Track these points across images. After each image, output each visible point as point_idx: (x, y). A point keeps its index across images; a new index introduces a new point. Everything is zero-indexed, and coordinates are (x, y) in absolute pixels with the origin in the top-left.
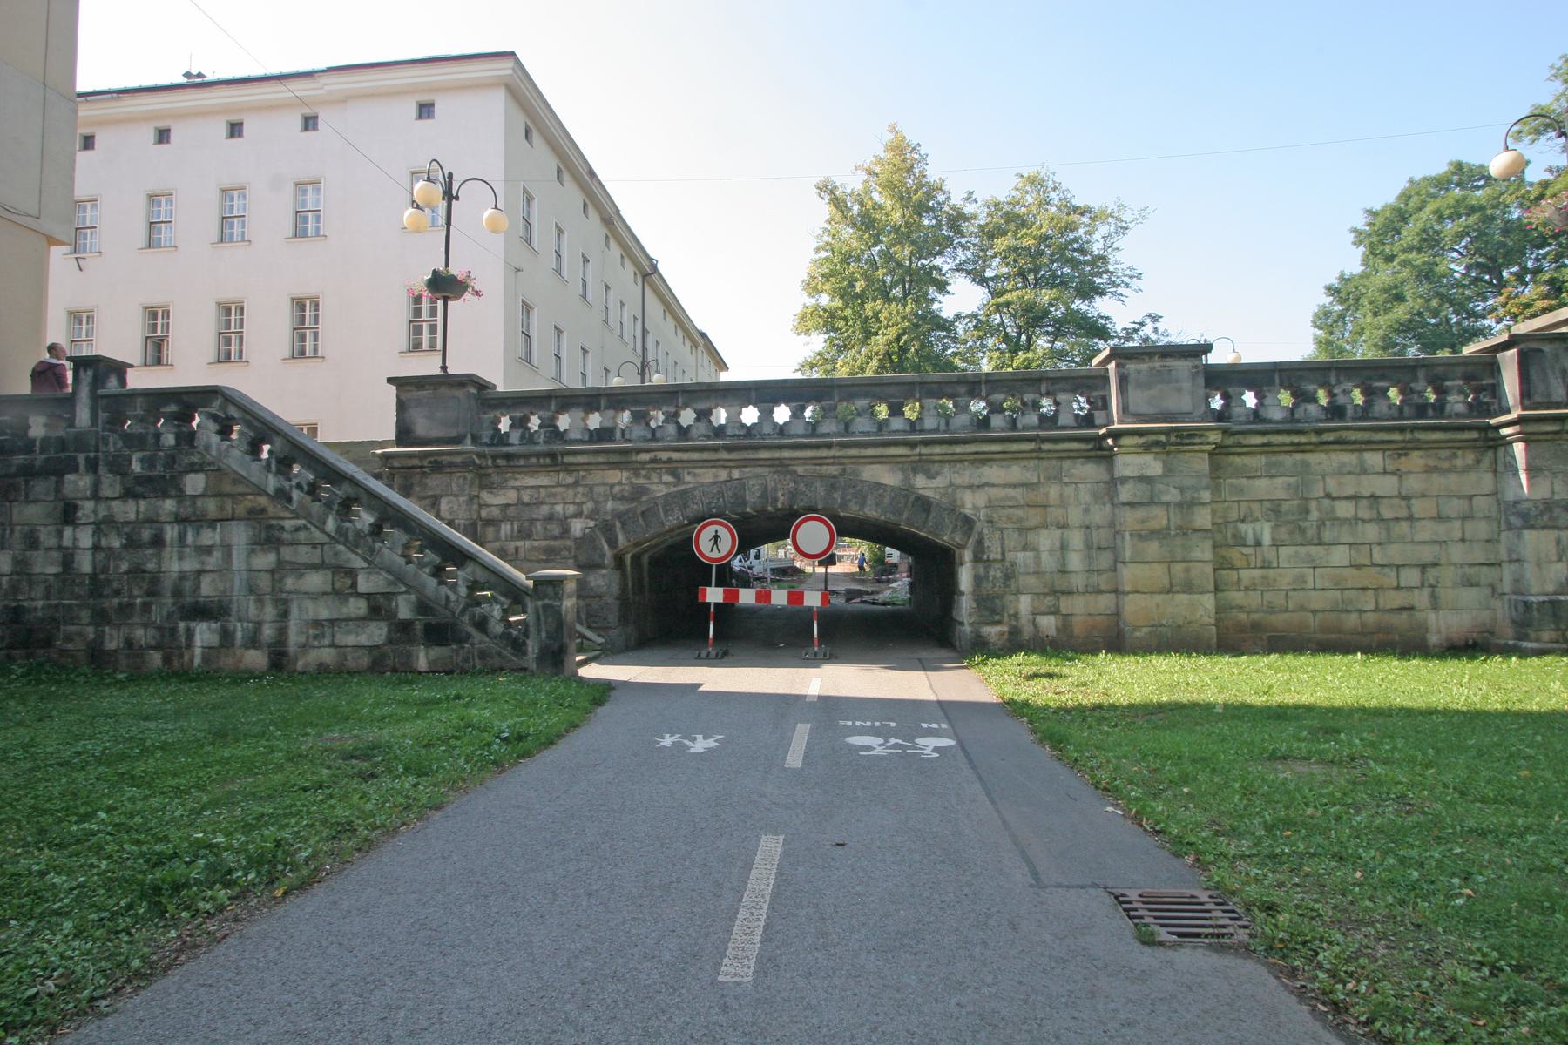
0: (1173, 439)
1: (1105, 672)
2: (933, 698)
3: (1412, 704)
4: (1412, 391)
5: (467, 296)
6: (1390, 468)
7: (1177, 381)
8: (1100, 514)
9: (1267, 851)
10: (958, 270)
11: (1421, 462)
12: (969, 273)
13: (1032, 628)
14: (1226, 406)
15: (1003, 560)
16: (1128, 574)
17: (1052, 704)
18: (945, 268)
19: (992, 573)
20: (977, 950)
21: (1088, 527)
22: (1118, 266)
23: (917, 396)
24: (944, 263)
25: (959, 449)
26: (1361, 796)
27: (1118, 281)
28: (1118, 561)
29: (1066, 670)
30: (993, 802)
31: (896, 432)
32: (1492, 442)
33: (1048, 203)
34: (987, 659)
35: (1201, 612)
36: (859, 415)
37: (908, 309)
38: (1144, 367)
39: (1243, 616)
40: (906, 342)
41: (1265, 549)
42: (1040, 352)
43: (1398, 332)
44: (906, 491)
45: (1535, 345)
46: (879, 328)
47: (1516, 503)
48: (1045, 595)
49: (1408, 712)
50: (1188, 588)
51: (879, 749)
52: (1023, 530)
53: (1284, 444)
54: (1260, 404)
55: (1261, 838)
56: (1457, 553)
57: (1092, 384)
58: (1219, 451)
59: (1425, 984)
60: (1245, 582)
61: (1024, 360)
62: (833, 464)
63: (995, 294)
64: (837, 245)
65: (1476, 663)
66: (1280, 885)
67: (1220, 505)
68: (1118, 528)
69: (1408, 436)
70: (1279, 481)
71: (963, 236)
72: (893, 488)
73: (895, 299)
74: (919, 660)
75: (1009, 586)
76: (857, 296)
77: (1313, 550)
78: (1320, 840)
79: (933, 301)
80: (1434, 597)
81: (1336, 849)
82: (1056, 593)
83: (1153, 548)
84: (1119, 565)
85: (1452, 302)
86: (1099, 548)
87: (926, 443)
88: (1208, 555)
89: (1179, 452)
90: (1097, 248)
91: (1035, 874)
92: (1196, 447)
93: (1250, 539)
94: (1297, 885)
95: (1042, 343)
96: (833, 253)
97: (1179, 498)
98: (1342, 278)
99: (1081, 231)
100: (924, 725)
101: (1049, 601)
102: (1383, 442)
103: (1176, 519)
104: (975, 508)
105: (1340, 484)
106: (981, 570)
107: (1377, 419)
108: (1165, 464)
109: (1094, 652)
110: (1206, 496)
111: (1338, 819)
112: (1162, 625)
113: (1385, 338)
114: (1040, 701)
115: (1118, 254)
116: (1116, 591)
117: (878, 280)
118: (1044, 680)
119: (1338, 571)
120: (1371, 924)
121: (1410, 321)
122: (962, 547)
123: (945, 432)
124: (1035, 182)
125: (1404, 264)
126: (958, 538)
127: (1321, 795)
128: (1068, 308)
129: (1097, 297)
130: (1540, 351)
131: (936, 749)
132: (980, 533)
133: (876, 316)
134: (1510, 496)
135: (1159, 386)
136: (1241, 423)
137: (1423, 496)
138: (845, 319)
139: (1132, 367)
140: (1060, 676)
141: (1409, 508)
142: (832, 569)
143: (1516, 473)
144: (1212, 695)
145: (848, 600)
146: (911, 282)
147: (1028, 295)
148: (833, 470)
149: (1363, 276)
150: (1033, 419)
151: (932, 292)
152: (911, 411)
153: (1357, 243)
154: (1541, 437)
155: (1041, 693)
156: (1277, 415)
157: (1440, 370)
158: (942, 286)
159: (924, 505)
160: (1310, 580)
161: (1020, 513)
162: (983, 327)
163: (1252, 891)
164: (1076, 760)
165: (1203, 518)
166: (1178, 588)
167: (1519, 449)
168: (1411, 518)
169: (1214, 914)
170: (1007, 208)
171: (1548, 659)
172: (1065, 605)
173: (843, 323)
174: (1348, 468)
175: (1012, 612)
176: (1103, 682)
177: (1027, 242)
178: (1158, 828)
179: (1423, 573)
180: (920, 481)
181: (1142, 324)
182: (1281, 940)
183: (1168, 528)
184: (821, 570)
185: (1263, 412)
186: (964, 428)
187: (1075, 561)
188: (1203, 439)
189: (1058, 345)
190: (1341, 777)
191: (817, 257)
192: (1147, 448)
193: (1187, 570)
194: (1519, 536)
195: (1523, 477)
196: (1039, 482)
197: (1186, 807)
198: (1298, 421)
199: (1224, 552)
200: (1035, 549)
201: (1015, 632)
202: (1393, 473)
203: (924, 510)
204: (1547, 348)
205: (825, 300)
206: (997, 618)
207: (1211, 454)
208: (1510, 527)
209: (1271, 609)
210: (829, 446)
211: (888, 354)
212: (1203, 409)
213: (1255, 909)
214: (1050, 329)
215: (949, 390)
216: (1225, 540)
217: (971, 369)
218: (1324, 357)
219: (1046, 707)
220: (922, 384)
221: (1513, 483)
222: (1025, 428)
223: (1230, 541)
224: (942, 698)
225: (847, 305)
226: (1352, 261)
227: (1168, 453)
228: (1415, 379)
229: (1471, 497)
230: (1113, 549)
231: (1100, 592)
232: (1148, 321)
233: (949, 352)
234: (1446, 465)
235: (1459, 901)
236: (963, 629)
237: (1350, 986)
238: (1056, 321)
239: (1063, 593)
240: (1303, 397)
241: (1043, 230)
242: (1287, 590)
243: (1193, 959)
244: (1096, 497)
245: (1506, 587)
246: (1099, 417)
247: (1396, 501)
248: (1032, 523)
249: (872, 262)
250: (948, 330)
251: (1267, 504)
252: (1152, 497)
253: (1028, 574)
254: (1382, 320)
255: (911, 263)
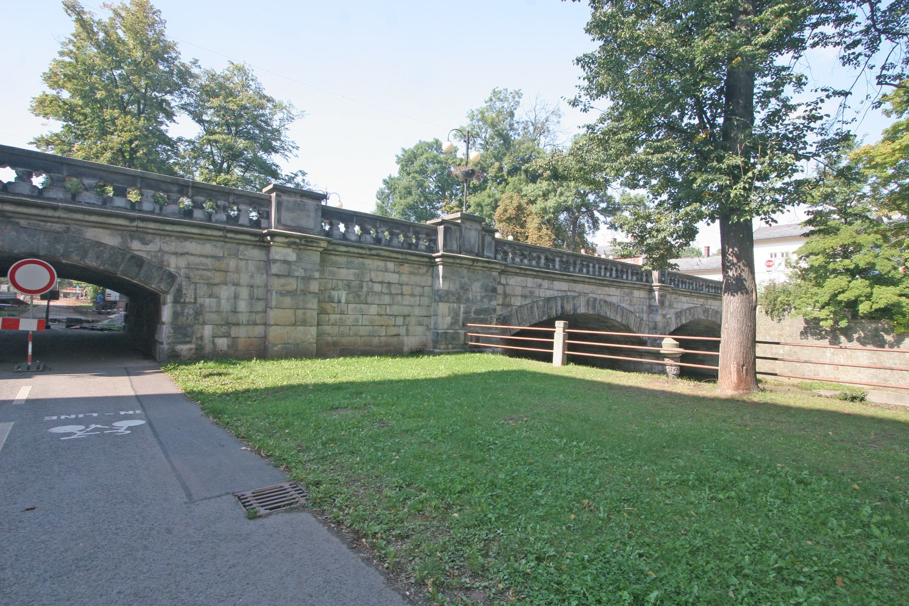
0: (303, 242)
1: (254, 371)
2: (132, 393)
3: (394, 378)
4: (408, 237)
5: (515, 111)
6: (396, 270)
7: (308, 211)
8: (259, 280)
9: (321, 456)
10: (182, 108)
11: (408, 269)
12: (190, 112)
13: (211, 346)
14: (331, 229)
15: (195, 303)
16: (273, 315)
17: (218, 391)
18: (173, 104)
19: (186, 311)
20: (140, 553)
21: (252, 286)
22: (287, 139)
23: (139, 185)
24: (174, 100)
25: (168, 228)
26: (366, 422)
27: (286, 147)
28: (268, 307)
29: (231, 371)
30: (167, 456)
31: (118, 208)
32: (432, 265)
33: (248, 87)
34: (178, 366)
35: (309, 336)
36: (86, 190)
37: (141, 123)
38: (291, 199)
39: (329, 339)
40: (137, 146)
41: (342, 304)
42: (235, 177)
43: (409, 209)
44: (123, 251)
45: (449, 226)
46: (115, 130)
47: (438, 291)
48: (222, 325)
49: (391, 382)
50: (304, 323)
51: (79, 433)
52: (210, 285)
53: (354, 253)
54: (346, 231)
55: (319, 450)
56: (417, 311)
57: (260, 203)
58: (325, 252)
59: (375, 501)
60: (332, 321)
61: (225, 179)
62: (57, 223)
63: (210, 132)
64: (81, 57)
65: (419, 359)
66: (325, 471)
67: (323, 280)
68: (269, 288)
69: (404, 257)
70: (352, 271)
71: (188, 87)
72: (112, 248)
73: (130, 112)
74: (125, 368)
75: (198, 320)
76: (96, 101)
77: (363, 306)
78: (345, 445)
79: (162, 123)
80: (407, 330)
81: (351, 448)
82: (228, 324)
83: (288, 301)
84: (268, 309)
85: (428, 201)
86: (258, 299)
87: (143, 220)
88: (315, 306)
89: (306, 249)
90: (275, 124)
91: (189, 496)
92: (314, 248)
93: (336, 300)
94: (332, 469)
95: (237, 172)
96: (77, 61)
97: (303, 275)
98: (390, 178)
99: (267, 111)
100: (122, 413)
101: (224, 329)
102: (395, 258)
103: (301, 286)
104: (178, 268)
105: (377, 275)
106: (179, 308)
107: (393, 247)
108: (298, 255)
109: (249, 359)
110: (317, 275)
111: (354, 434)
112: (289, 344)
113: (403, 210)
114: (211, 390)
115: (287, 132)
116: (265, 324)
117: (117, 95)
118: (216, 378)
119: (372, 317)
120: (359, 481)
121: (414, 205)
122: (167, 293)
123: (159, 214)
124: (240, 70)
125: (414, 178)
126: (163, 286)
127: (349, 424)
128: (255, 155)
129: (273, 153)
130: (450, 228)
131: (129, 428)
132: (180, 286)
133: (113, 120)
134: (436, 288)
135: (298, 212)
136: (337, 239)
137: (407, 284)
138: (85, 116)
139: (285, 198)
140: (226, 374)
141: (402, 289)
142: (52, 303)
143: (439, 279)
144: (310, 380)
145: (68, 327)
146: (145, 105)
147: (230, 140)
148: (57, 227)
149: (399, 179)
150: (223, 217)
151: (161, 117)
152: (133, 196)
153: (398, 163)
154: (212, 238)
155: (212, 385)
156: (353, 238)
157: (418, 229)
158: (170, 115)
159: (138, 262)
160: (361, 321)
161: (209, 274)
162: (198, 151)
163: (311, 477)
164: (228, 423)
165: (314, 286)
166: (299, 323)
167: (441, 267)
168: (402, 294)
169: (291, 493)
170: (221, 80)
171: (442, 356)
172: (234, 332)
173: (81, 117)
174: (380, 269)
175: (199, 335)
176: (252, 377)
177: (232, 106)
178: (269, 454)
179: (404, 319)
180: (136, 245)
181: (296, 175)
182: (320, 498)
183: (296, 290)
184: (45, 303)
185: (348, 236)
186: (173, 214)
187: (242, 306)
188: (318, 245)
189: (247, 175)
190: (359, 414)
191: (61, 59)
192: (289, 245)
193: (304, 314)
194: (438, 305)
195: (441, 280)
196: (223, 257)
197: (286, 440)
198: (362, 242)
199: (323, 305)
200: (218, 297)
201: (200, 348)
202: (397, 273)
203: (137, 266)
204: (453, 227)
205: (65, 95)
206: (188, 339)
207: (321, 253)
208: (435, 301)
209: (343, 335)
210: (55, 208)
211: (121, 152)
212: (319, 229)
213: (310, 486)
214: (243, 164)
215: (164, 187)
216: (325, 299)
217: (188, 177)
218: (379, 214)
219: (215, 394)
220: (143, 178)
221: (437, 281)
222: (216, 222)
223: (327, 299)
224: (139, 394)
225: (87, 106)
226: (394, 170)
227: (300, 249)
228: (409, 231)
229: (424, 287)
230: (266, 300)
231: (256, 324)
232: (299, 174)
233: (171, 161)
234: (416, 271)
235: (393, 462)
236: (162, 346)
237: (346, 512)
238: (247, 160)
239: (234, 324)
240: (365, 231)
241: (243, 103)
242: (350, 326)
243: (278, 519)
244: (258, 269)
245: (432, 326)
246: (264, 223)
247: (397, 286)
248: (217, 281)
249: (113, 80)
250: (172, 146)
251: (345, 282)
252: (289, 272)
253: (212, 312)
254: (403, 201)
255: (146, 91)
